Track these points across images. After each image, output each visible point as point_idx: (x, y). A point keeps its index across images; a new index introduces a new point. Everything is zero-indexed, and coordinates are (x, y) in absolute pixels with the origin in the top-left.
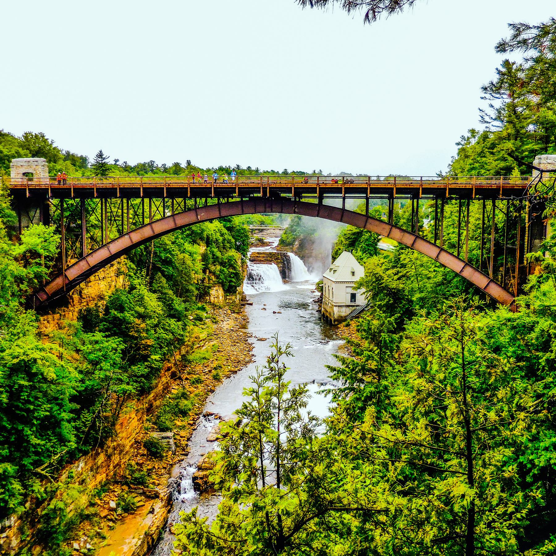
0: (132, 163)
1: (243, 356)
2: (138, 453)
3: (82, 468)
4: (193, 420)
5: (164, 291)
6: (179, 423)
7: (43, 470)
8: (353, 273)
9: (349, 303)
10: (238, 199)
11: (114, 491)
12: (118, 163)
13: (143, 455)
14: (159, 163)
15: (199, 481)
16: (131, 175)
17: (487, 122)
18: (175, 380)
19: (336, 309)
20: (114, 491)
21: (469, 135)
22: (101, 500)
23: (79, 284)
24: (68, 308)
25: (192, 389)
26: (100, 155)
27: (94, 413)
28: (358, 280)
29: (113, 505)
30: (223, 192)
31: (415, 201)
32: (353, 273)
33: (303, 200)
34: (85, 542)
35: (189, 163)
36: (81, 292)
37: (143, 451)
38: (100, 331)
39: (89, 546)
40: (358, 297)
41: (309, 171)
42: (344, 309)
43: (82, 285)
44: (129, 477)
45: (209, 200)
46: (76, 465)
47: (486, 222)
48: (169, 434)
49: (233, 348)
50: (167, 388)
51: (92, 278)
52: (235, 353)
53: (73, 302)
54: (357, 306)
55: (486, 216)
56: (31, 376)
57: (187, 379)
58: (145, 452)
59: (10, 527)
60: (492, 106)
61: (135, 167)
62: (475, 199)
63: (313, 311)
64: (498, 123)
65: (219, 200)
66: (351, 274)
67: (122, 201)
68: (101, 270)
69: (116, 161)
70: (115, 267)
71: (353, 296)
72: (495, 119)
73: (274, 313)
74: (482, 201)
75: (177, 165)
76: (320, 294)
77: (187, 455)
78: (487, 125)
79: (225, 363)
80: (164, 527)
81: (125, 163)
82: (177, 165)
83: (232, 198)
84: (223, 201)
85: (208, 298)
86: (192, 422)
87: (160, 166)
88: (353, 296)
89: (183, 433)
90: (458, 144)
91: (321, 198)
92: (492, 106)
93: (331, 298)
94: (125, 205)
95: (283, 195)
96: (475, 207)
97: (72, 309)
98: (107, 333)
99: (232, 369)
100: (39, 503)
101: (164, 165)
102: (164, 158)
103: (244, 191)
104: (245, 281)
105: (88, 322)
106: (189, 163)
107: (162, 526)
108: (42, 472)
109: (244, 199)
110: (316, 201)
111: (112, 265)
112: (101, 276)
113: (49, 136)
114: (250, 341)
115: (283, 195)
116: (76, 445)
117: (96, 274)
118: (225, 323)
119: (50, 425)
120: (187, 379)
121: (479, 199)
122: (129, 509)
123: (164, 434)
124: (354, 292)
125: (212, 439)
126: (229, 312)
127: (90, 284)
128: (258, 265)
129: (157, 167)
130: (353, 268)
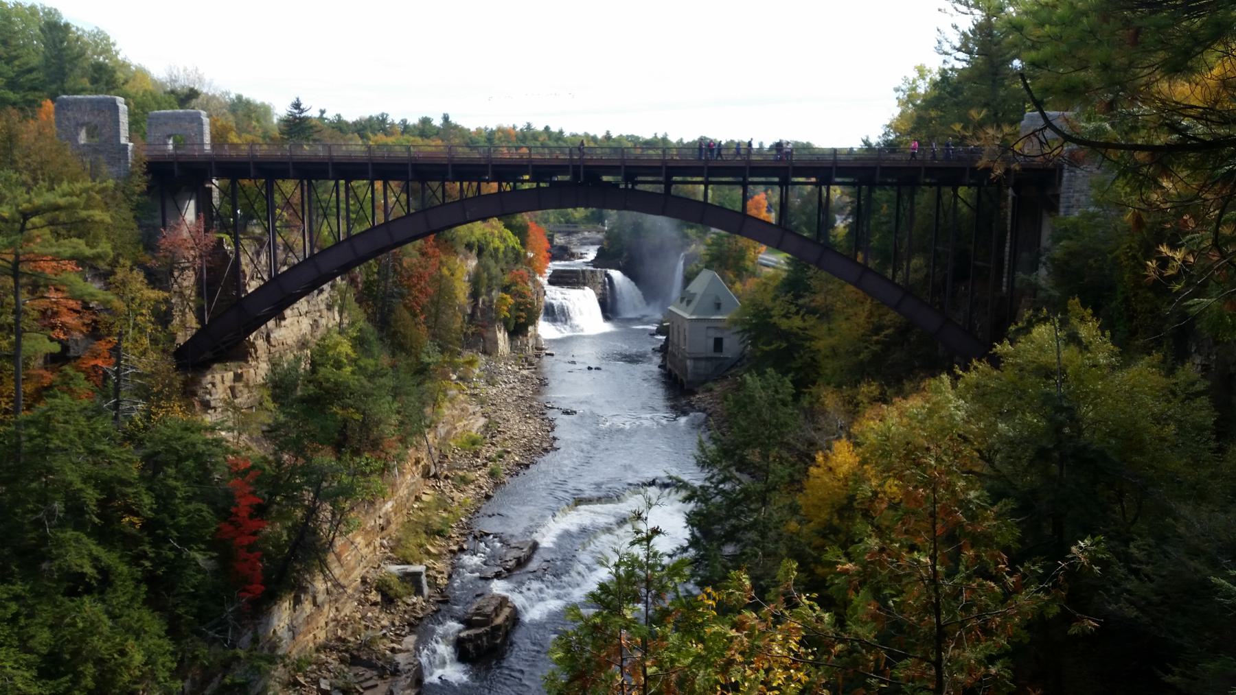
0: (350, 117)
2: (367, 600)
7: (210, 629)
9: (711, 353)
10: (534, 185)
13: (375, 604)
17: (946, 53)
19: (689, 363)
21: (916, 75)
23: (265, 322)
24: (247, 362)
26: (297, 105)
30: (505, 171)
31: (824, 189)
33: (640, 187)
35: (446, 118)
36: (268, 337)
37: (374, 596)
42: (703, 364)
43: (271, 324)
44: (352, 639)
45: (483, 185)
47: (942, 221)
51: (288, 312)
53: (256, 351)
55: (941, 214)
57: (447, 477)
58: (379, 599)
60: (956, 27)
61: (355, 124)
62: (925, 184)
63: (653, 366)
64: (962, 55)
65: (500, 186)
67: (337, 185)
68: (303, 300)
69: (323, 112)
70: (325, 295)
71: (718, 343)
72: (959, 50)
73: (590, 368)
74: (935, 188)
75: (426, 121)
76: (874, 195)
78: (946, 57)
83: (523, 181)
84: (507, 187)
87: (397, 122)
88: (718, 343)
89: (439, 565)
90: (897, 90)
91: (668, 184)
92: (956, 27)
94: (342, 189)
95: (605, 178)
96: (925, 197)
97: (254, 363)
101: (404, 121)
102: (405, 109)
103: (541, 171)
104: (541, 316)
106: (446, 118)
109: (542, 185)
110: (660, 189)
111: (321, 291)
112: (303, 310)
113: (246, 95)
114: (550, 414)
115: (605, 178)
117: (295, 306)
120: (447, 477)
121: (930, 185)
124: (719, 335)
127: (283, 323)
128: (565, 290)
129: (392, 124)
130: (717, 298)
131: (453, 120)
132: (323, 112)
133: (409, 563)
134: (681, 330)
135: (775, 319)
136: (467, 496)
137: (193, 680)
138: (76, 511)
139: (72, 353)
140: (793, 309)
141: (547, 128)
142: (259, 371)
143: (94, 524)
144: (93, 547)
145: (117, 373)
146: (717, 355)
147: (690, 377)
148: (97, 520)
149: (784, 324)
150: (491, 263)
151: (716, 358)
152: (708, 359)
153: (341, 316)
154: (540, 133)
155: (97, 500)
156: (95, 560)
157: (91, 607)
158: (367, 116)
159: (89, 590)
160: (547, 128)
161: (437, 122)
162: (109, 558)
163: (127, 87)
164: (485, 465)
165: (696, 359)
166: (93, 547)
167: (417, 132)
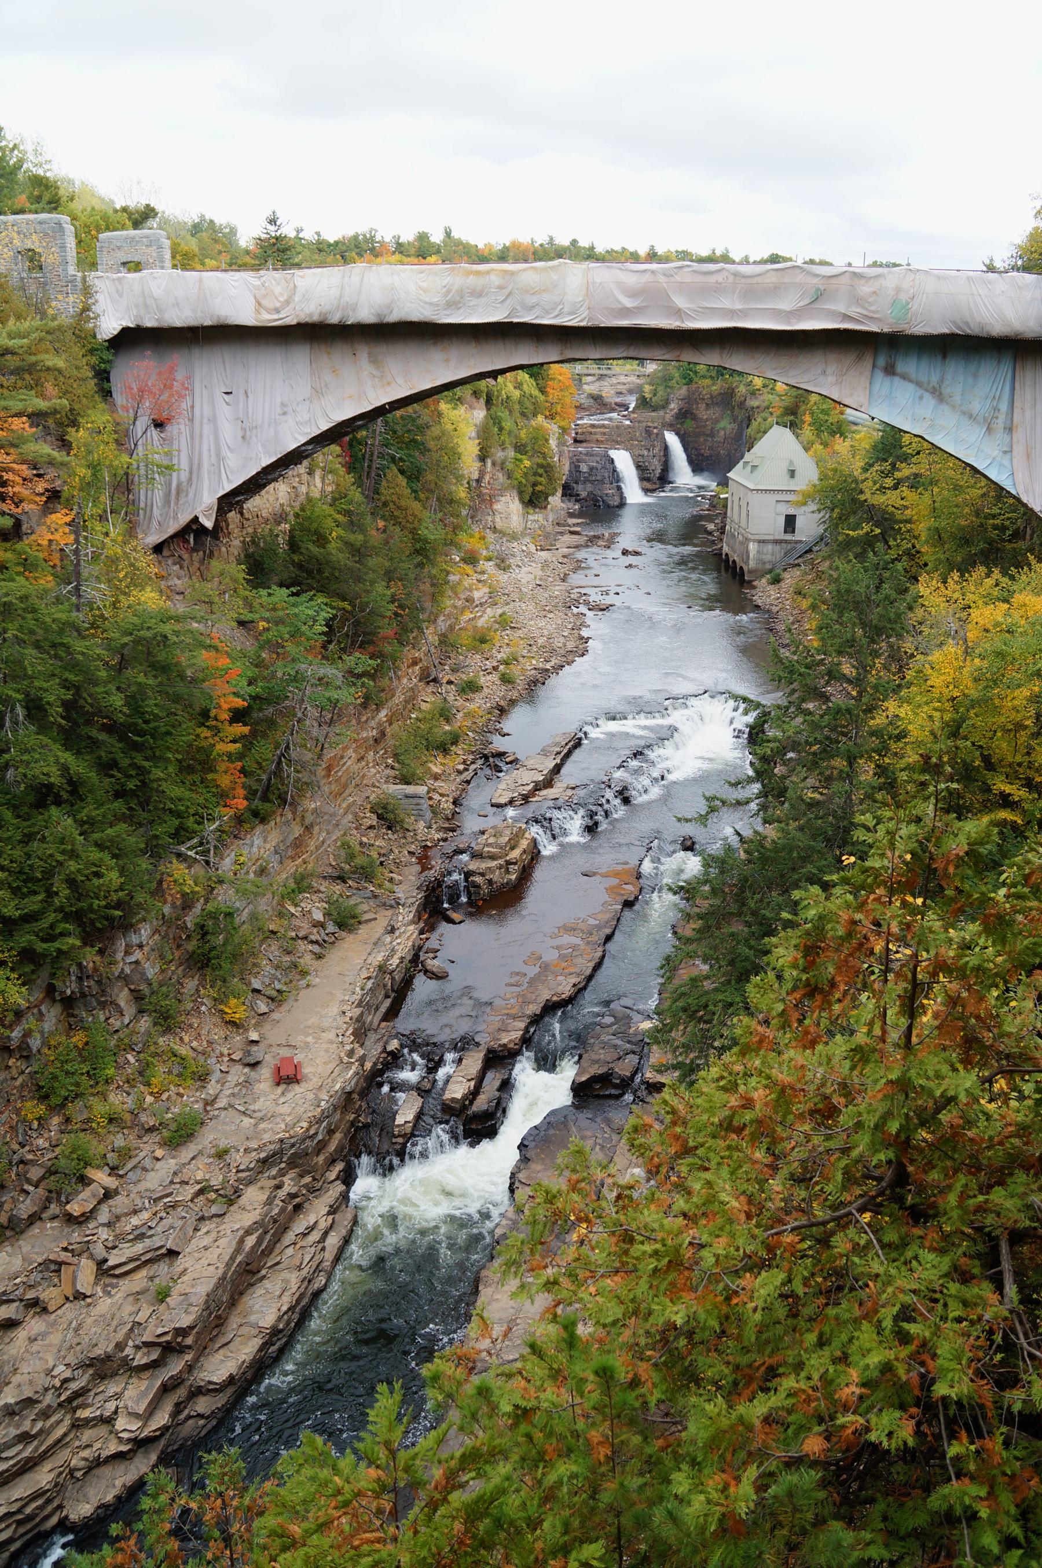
0: (331, 236)
1: (562, 640)
3: (259, 848)
4: (464, 762)
5: (403, 503)
6: (436, 769)
7: (189, 849)
8: (792, 473)
11: (319, 891)
12: (301, 235)
14: (386, 234)
15: (478, 879)
16: (131, 1405)
18: (428, 683)
19: (752, 547)
20: (319, 891)
22: (296, 905)
25: (460, 703)
27: (277, 746)
28: (804, 488)
29: (318, 916)
32: (792, 473)
34: (274, 978)
35: (448, 234)
38: (281, 585)
39: (278, 986)
40: (799, 523)
41: (473, 243)
46: (247, 841)
48: (422, 790)
49: (542, 623)
50: (411, 701)
52: (546, 632)
53: (228, 525)
54: (797, 542)
56: (162, 669)
57: (450, 682)
59: (141, 946)
61: (337, 243)
66: (787, 477)
71: (790, 522)
75: (423, 237)
77: (453, 830)
79: (525, 652)
80: (415, 959)
81: (318, 234)
82: (423, 237)
85: (490, 518)
86: (461, 767)
87: (387, 239)
88: (790, 522)
93: (743, 524)
98: (294, 590)
99: (541, 665)
100: (187, 902)
105: (258, 569)
106: (448, 234)
107: (409, 958)
108: (189, 853)
116: (245, 803)
118: (524, 570)
119: (198, 765)
120: (450, 682)
122: (346, 921)
123: (410, 789)
124: (791, 512)
125: (503, 800)
126: (533, 548)
129: (382, 243)
130: (791, 462)
131: (455, 234)
132: (299, 231)
133: (408, 783)
134: (744, 504)
135: (867, 495)
136: (478, 704)
137: (173, 904)
138: (35, 709)
139: (24, 528)
140: (889, 482)
141: (574, 242)
142: (231, 549)
143: (60, 726)
144: (60, 754)
145: (76, 552)
146: (788, 537)
147: (752, 564)
148: (63, 722)
149: (879, 500)
150: (504, 414)
151: (786, 541)
152: (777, 542)
153: (323, 482)
154: (568, 248)
155: (215, 771)
156: (65, 768)
157: (61, 822)
158: (351, 233)
159: (58, 802)
160: (574, 242)
161: (437, 238)
162: (79, 767)
163: (72, 206)
164: (495, 668)
165: (762, 542)
166: (60, 754)
167: (412, 251)
